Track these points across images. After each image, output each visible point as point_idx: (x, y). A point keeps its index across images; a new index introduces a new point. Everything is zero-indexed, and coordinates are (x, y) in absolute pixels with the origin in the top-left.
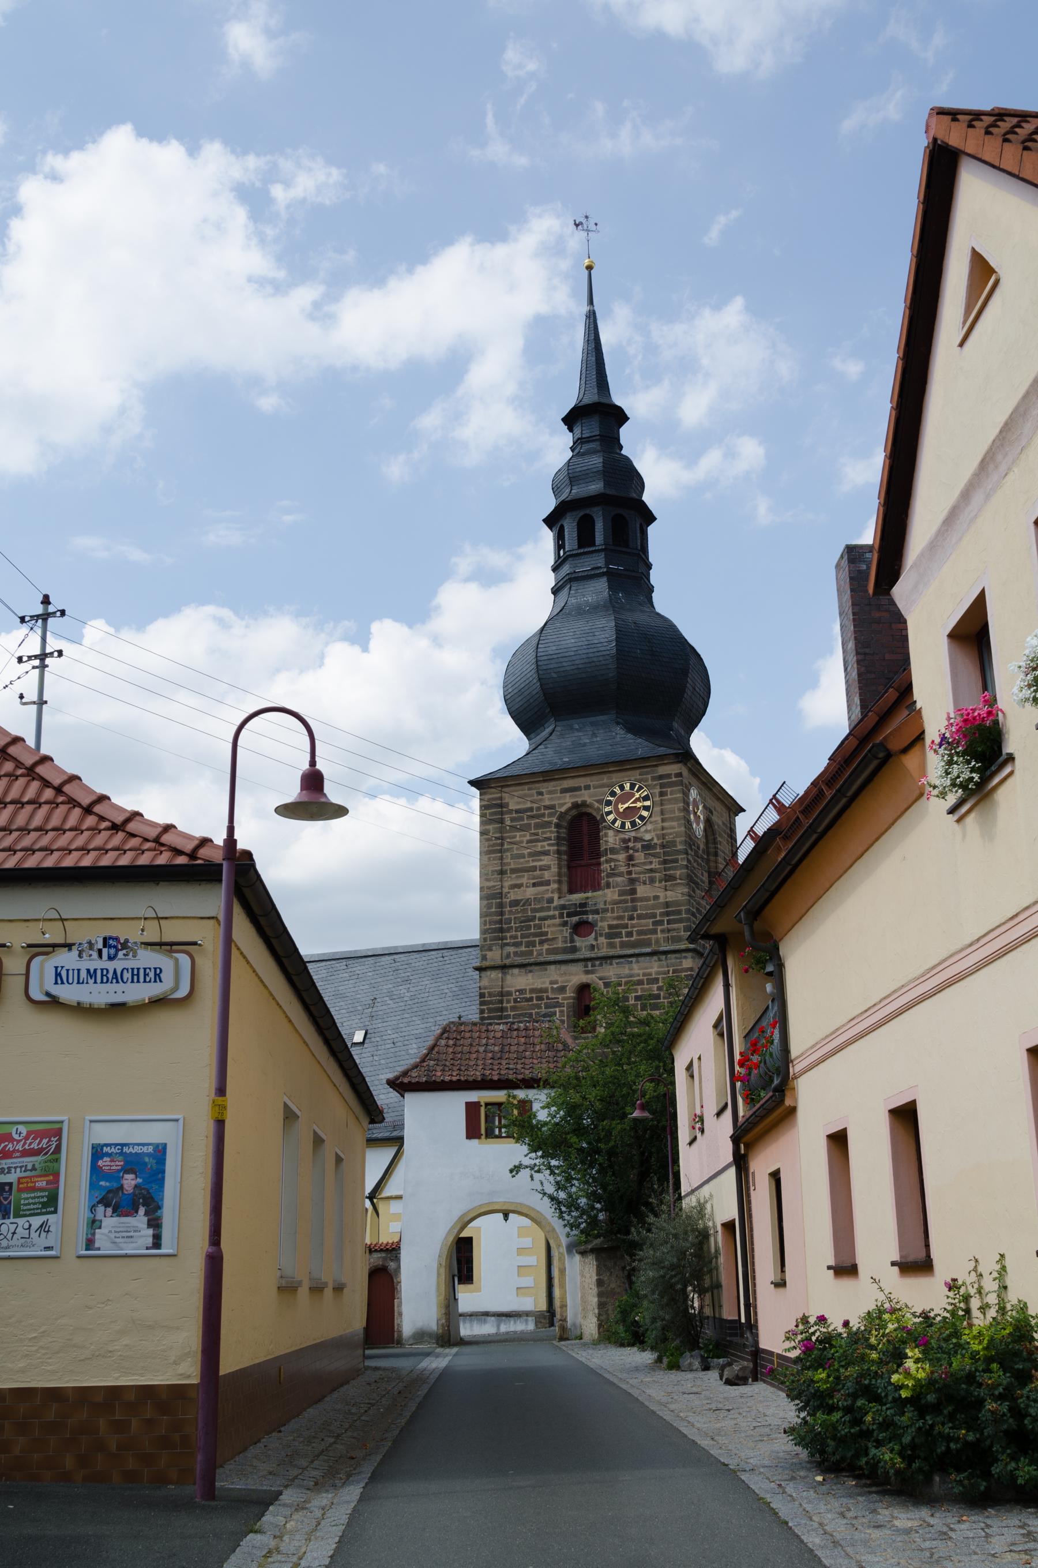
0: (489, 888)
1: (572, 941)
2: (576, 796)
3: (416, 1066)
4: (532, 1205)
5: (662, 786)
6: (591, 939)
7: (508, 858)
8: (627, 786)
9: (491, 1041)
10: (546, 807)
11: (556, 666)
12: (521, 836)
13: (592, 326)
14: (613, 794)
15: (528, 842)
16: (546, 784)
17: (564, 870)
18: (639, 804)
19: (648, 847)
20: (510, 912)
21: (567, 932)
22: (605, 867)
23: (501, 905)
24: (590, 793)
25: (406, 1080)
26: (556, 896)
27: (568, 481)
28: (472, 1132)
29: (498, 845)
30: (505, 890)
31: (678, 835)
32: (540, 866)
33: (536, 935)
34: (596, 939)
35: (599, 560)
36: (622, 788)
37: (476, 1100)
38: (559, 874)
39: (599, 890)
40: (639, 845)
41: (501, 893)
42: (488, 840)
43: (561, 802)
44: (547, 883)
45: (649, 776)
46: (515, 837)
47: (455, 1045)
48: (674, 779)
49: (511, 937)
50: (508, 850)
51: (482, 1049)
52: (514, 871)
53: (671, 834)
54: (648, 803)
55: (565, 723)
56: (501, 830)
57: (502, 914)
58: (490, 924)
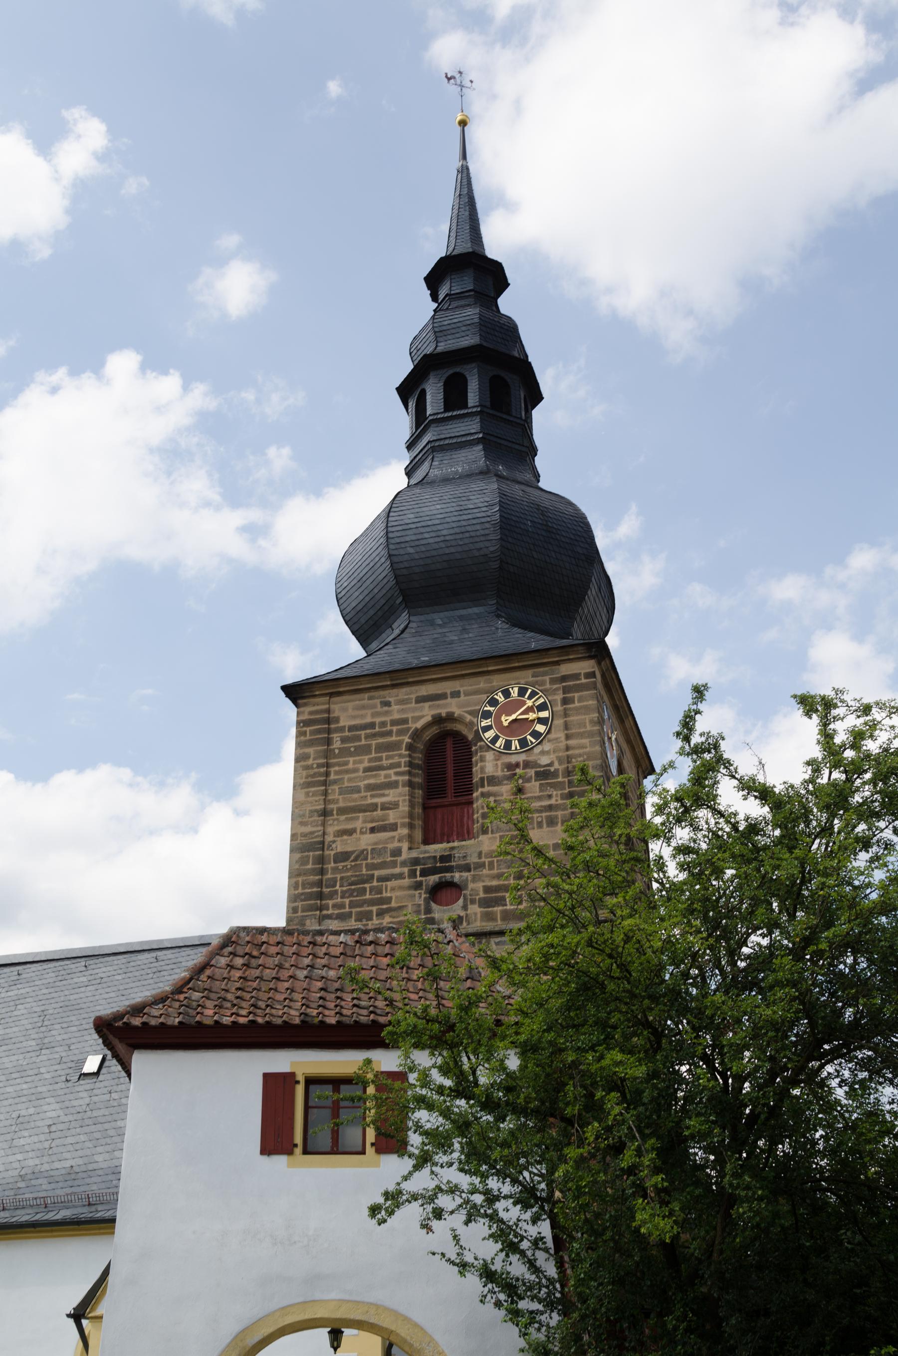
0: (304, 835)
1: (428, 910)
2: (438, 706)
3: (161, 999)
4: (402, 1309)
5: (566, 690)
6: (456, 910)
7: (334, 792)
8: (514, 692)
9: (320, 962)
10: (394, 723)
11: (414, 538)
12: (355, 762)
13: (465, 180)
14: (493, 702)
15: (367, 770)
16: (395, 691)
17: (418, 810)
18: (532, 716)
19: (544, 774)
20: (335, 870)
21: (420, 898)
22: (479, 804)
23: (321, 860)
24: (461, 701)
25: (137, 1022)
26: (405, 846)
27: (432, 337)
28: (275, 1140)
29: (320, 775)
30: (329, 838)
31: (590, 757)
32: (383, 804)
33: (372, 903)
34: (465, 908)
35: (473, 426)
36: (506, 694)
37: (286, 1069)
38: (411, 816)
39: (470, 839)
40: (531, 772)
41: (323, 843)
42: (307, 768)
43: (417, 714)
44: (393, 827)
45: (547, 678)
46: (347, 763)
47: (247, 965)
48: (584, 681)
49: (334, 906)
50: (335, 782)
51: (301, 974)
52: (342, 811)
53: (580, 755)
54: (544, 714)
55: (422, 618)
56: (327, 754)
57: (322, 872)
58: (304, 888)
